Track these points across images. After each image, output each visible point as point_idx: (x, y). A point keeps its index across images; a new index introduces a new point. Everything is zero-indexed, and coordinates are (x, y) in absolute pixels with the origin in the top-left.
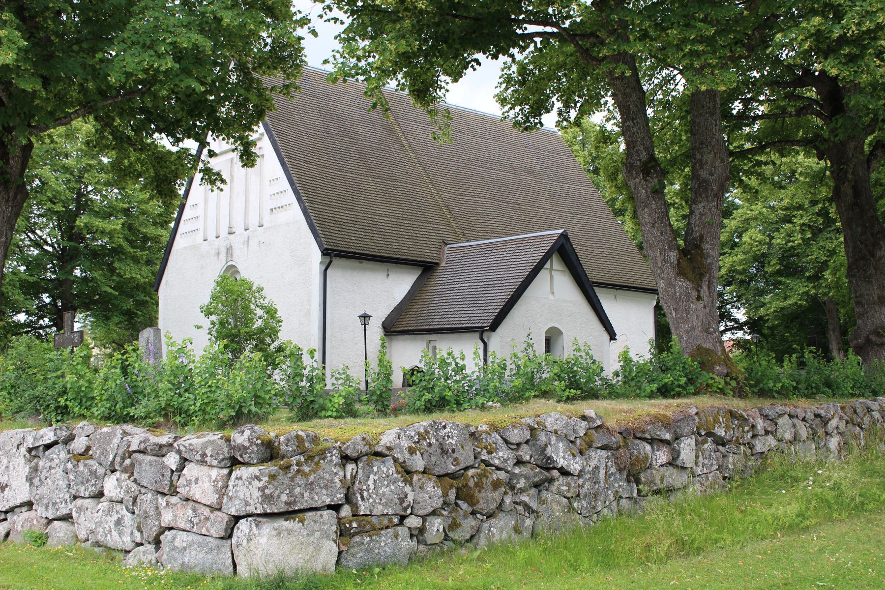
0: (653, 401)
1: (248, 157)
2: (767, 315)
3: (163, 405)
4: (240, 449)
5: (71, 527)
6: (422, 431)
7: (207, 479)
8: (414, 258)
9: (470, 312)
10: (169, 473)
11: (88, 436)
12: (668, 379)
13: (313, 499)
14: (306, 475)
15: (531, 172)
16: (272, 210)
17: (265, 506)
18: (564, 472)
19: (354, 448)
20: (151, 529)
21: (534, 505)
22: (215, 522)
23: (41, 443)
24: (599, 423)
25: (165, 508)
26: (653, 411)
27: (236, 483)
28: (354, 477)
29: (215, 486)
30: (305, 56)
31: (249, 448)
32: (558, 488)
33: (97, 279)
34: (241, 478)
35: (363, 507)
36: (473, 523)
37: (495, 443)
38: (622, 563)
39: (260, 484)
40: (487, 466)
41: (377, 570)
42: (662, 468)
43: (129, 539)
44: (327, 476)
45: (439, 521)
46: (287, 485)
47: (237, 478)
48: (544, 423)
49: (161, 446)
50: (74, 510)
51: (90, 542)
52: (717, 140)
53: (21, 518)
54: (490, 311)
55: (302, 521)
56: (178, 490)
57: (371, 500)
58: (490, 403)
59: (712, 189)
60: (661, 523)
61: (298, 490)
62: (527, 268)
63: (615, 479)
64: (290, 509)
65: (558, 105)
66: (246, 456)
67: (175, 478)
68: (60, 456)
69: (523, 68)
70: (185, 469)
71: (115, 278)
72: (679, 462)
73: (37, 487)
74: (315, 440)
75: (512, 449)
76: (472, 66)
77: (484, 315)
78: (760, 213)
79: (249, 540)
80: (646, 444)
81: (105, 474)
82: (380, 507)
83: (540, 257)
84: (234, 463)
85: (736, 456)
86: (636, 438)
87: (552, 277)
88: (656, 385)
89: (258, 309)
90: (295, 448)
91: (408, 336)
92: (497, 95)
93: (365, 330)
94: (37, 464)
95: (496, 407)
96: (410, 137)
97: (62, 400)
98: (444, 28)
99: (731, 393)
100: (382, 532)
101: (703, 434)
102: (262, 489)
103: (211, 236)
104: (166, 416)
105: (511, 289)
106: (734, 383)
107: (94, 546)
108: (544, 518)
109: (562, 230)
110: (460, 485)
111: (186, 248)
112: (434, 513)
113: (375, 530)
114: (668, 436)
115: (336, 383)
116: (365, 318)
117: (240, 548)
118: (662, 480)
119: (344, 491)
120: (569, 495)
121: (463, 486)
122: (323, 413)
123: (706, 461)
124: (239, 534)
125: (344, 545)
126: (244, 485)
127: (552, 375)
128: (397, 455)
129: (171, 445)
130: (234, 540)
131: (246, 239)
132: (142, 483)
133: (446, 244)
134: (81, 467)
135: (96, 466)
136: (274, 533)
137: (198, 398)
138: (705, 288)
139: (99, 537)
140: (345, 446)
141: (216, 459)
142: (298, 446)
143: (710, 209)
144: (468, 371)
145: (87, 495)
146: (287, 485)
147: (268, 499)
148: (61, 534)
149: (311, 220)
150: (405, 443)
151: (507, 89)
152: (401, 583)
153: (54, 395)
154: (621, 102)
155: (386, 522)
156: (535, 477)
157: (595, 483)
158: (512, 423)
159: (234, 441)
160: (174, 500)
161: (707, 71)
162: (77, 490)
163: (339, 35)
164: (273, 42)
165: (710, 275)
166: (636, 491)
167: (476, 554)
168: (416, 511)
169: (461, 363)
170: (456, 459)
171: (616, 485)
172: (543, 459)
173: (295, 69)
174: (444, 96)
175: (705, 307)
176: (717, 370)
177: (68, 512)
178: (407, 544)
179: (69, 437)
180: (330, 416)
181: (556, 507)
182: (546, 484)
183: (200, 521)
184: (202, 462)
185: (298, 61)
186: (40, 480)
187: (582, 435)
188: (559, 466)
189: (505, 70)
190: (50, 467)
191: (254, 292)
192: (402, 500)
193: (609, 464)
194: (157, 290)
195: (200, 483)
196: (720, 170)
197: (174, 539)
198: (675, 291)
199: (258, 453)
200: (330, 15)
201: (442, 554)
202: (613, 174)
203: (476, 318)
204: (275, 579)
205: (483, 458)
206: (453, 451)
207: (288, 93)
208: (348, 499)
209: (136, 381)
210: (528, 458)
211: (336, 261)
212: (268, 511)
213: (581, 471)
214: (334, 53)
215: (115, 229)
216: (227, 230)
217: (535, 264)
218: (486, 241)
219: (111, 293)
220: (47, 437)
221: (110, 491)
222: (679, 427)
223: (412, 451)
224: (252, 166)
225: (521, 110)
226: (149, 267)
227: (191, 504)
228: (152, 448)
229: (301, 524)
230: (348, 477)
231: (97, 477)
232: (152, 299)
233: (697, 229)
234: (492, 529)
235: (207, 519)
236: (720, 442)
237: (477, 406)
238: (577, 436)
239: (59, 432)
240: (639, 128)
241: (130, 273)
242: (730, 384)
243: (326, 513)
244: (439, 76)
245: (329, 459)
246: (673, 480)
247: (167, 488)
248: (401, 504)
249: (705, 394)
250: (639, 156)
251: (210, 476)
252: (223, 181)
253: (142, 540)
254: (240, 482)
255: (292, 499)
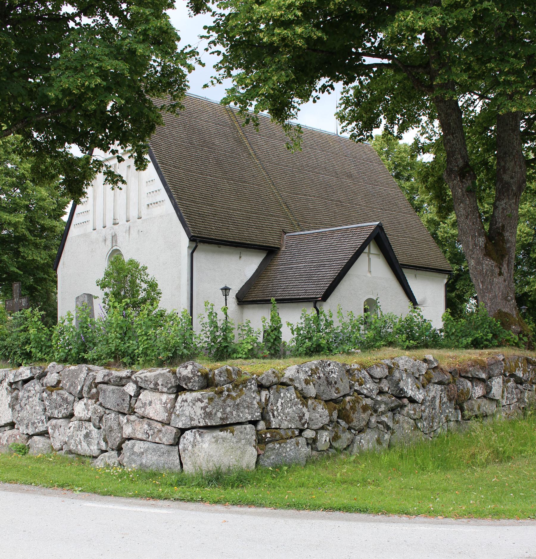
0: (469, 351)
1: (140, 164)
2: (531, 291)
3: (113, 349)
4: (185, 379)
5: (47, 441)
6: (314, 367)
7: (159, 402)
8: (261, 244)
9: (306, 286)
10: (128, 398)
11: (58, 373)
12: (479, 334)
13: (239, 416)
14: (234, 399)
15: (350, 176)
16: (148, 205)
17: (207, 420)
18: (412, 400)
19: (268, 379)
20: (115, 440)
21: (391, 424)
22: (166, 433)
23: (20, 379)
24: (436, 364)
25: (126, 424)
26: (473, 357)
27: (182, 404)
28: (267, 401)
29: (165, 407)
30: (188, 82)
31: (192, 379)
32: (408, 412)
33: (5, 261)
34: (186, 401)
35: (274, 423)
36: (349, 436)
37: (364, 378)
38: (455, 466)
39: (202, 405)
40: (358, 394)
41: (285, 468)
42: (479, 400)
43: (96, 447)
44: (248, 399)
45: (326, 433)
46: (221, 406)
47: (183, 401)
48: (398, 364)
49: (121, 378)
50: (50, 427)
51: (64, 451)
52: (517, 151)
53: (5, 435)
54: (322, 285)
55: (232, 432)
56: (135, 410)
57: (280, 418)
58: (353, 350)
59: (513, 189)
60: (482, 438)
61: (228, 409)
62: (351, 252)
63: (447, 407)
64: (224, 423)
65: (384, 122)
66: (190, 385)
67: (133, 401)
68: (36, 388)
69: (358, 93)
70: (141, 395)
71: (20, 260)
72: (491, 395)
73: (18, 411)
74: (239, 373)
75: (376, 383)
76: (328, 91)
77: (317, 288)
78: (528, 210)
79: (194, 445)
80: (468, 381)
81: (74, 401)
82: (286, 423)
83: (361, 244)
84: (179, 389)
85: (530, 392)
86: (461, 376)
87: (369, 259)
88: (471, 339)
89: (142, 283)
90: (226, 378)
91: (256, 305)
92: (337, 113)
93: (226, 300)
94: (17, 395)
95: (357, 353)
96: (255, 147)
97: (28, 348)
98: (304, 59)
99: (524, 346)
100: (288, 441)
101: (507, 375)
102: (204, 408)
103: (99, 226)
104: (115, 358)
105: (338, 268)
106: (525, 339)
107: (67, 453)
108: (398, 434)
109: (378, 222)
110: (341, 408)
111: (78, 236)
112: (323, 428)
113: (283, 439)
114: (484, 376)
115: (241, 333)
116: (226, 290)
117: (186, 451)
118: (479, 408)
119: (260, 410)
120: (415, 417)
121: (342, 409)
122: (235, 355)
123: (509, 396)
124: (185, 442)
125: (261, 450)
126: (189, 405)
127: (395, 329)
128: (297, 385)
129: (129, 378)
130: (181, 447)
131: (128, 229)
132: (106, 406)
133: (285, 233)
134: (54, 396)
135: (66, 395)
136: (213, 440)
137: (140, 344)
138: (505, 266)
139: (71, 447)
140: (260, 377)
141: (166, 387)
142: (228, 377)
143: (510, 205)
144: (335, 325)
145: (60, 416)
146: (221, 406)
147: (208, 415)
148: (40, 446)
149: (180, 213)
150: (302, 376)
151: (345, 108)
152: (304, 478)
153: (19, 345)
154: (443, 120)
155: (290, 434)
156: (392, 403)
157: (432, 409)
158: (375, 363)
159: (180, 374)
160: (132, 418)
161: (517, 97)
162: (52, 413)
163: (217, 65)
164: (162, 70)
165: (509, 257)
166: (460, 416)
167: (353, 458)
168: (310, 426)
169: (330, 319)
170: (337, 389)
171: (447, 411)
172: (397, 391)
173: (180, 92)
174: (296, 114)
175: (505, 281)
176: (513, 329)
177: (44, 429)
178: (305, 450)
179: (42, 374)
180: (240, 358)
181: (406, 426)
182: (399, 409)
183: (154, 433)
184: (155, 389)
185: (182, 86)
186: (21, 406)
187: (424, 373)
188: (409, 396)
189: (344, 94)
190: (28, 396)
191: (140, 270)
192: (301, 418)
193: (443, 395)
194: (56, 270)
195: (153, 405)
196: (519, 175)
197: (133, 446)
198: (483, 268)
199: (199, 382)
200: (214, 48)
201: (328, 458)
202: (425, 177)
203: (311, 291)
204: (214, 473)
205: (356, 388)
206: (336, 383)
207: (174, 112)
208: (264, 417)
209: (86, 332)
210: (387, 389)
211: (201, 246)
212: (209, 424)
213: (423, 400)
214: (213, 79)
215: (19, 222)
216: (112, 222)
217: (357, 249)
218: (317, 231)
219: (17, 273)
220: (25, 374)
221: (79, 413)
222: (492, 369)
223: (307, 382)
224: (145, 169)
225: (357, 125)
226: (47, 252)
227: (146, 420)
228: (115, 379)
229: (231, 434)
230: (263, 400)
231: (68, 403)
232: (49, 276)
233: (500, 220)
234: (362, 441)
235: (160, 431)
236: (519, 381)
237: (344, 352)
238: (421, 374)
239: (33, 370)
240: (458, 141)
241: (32, 256)
242: (523, 340)
243: (248, 426)
244: (293, 98)
245: (249, 387)
246: (486, 408)
247: (127, 409)
248: (300, 421)
249: (505, 346)
250: (457, 163)
251: (161, 400)
252: (124, 182)
253: (107, 448)
254: (186, 404)
255: (225, 416)
